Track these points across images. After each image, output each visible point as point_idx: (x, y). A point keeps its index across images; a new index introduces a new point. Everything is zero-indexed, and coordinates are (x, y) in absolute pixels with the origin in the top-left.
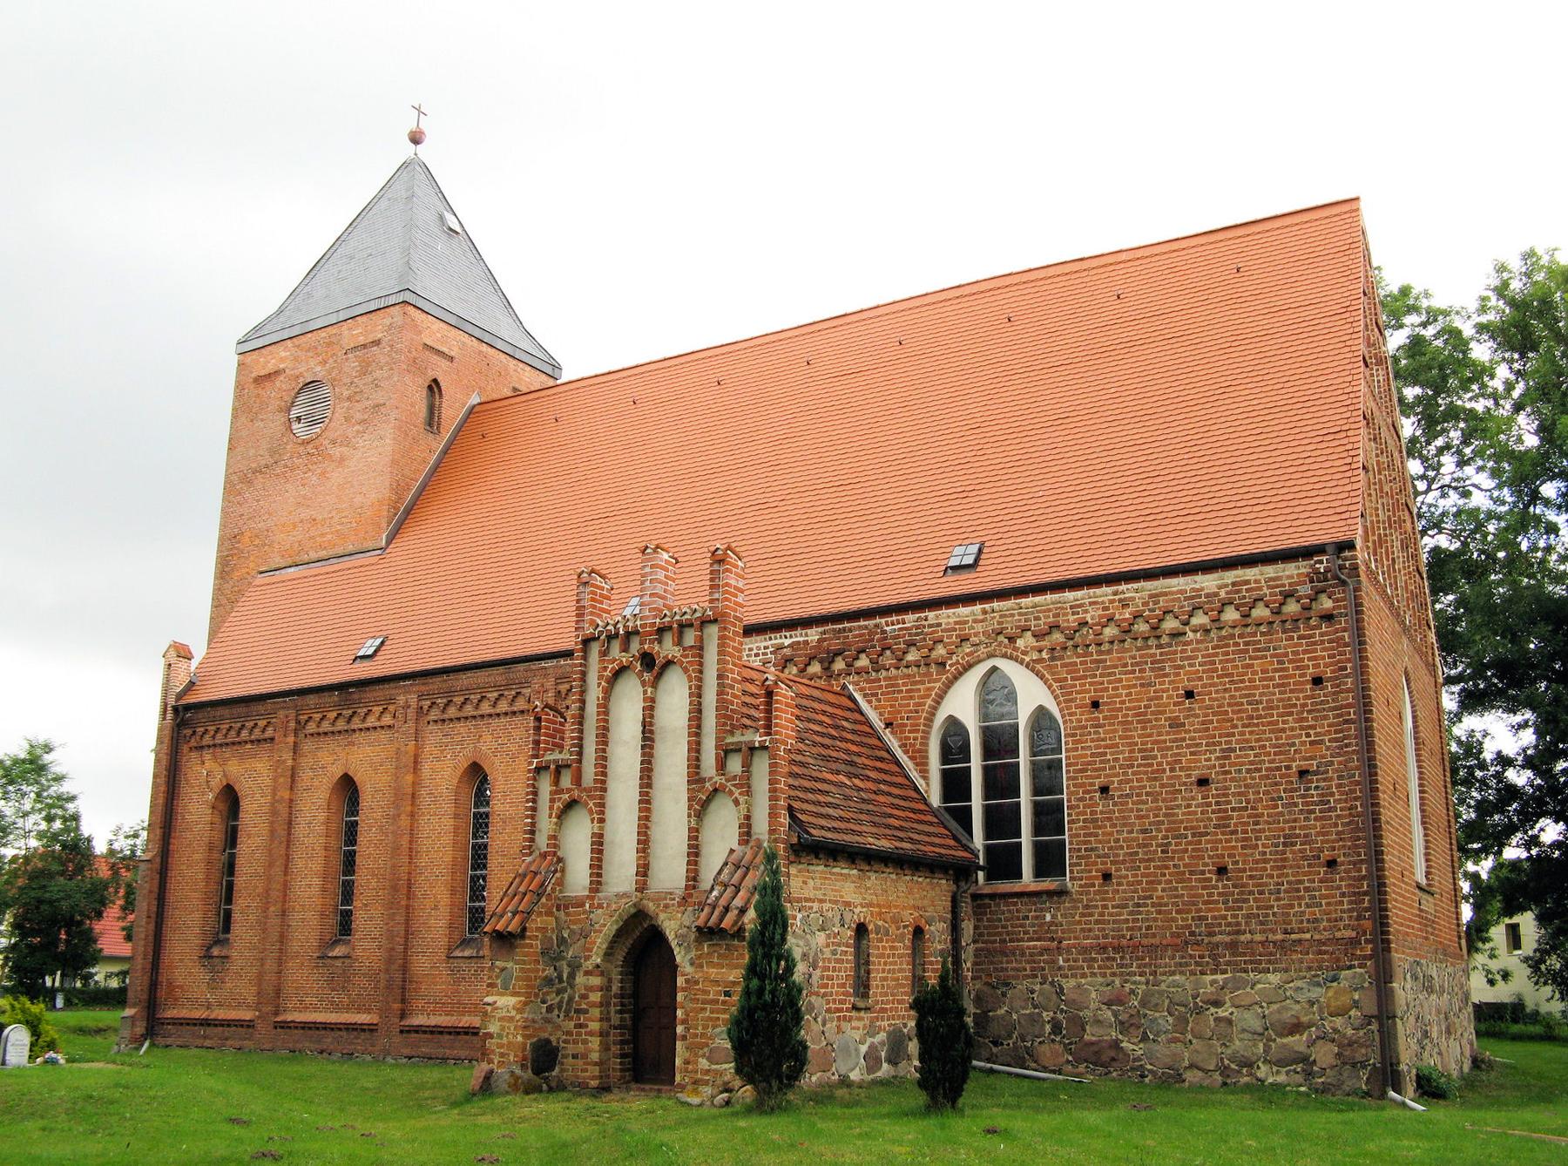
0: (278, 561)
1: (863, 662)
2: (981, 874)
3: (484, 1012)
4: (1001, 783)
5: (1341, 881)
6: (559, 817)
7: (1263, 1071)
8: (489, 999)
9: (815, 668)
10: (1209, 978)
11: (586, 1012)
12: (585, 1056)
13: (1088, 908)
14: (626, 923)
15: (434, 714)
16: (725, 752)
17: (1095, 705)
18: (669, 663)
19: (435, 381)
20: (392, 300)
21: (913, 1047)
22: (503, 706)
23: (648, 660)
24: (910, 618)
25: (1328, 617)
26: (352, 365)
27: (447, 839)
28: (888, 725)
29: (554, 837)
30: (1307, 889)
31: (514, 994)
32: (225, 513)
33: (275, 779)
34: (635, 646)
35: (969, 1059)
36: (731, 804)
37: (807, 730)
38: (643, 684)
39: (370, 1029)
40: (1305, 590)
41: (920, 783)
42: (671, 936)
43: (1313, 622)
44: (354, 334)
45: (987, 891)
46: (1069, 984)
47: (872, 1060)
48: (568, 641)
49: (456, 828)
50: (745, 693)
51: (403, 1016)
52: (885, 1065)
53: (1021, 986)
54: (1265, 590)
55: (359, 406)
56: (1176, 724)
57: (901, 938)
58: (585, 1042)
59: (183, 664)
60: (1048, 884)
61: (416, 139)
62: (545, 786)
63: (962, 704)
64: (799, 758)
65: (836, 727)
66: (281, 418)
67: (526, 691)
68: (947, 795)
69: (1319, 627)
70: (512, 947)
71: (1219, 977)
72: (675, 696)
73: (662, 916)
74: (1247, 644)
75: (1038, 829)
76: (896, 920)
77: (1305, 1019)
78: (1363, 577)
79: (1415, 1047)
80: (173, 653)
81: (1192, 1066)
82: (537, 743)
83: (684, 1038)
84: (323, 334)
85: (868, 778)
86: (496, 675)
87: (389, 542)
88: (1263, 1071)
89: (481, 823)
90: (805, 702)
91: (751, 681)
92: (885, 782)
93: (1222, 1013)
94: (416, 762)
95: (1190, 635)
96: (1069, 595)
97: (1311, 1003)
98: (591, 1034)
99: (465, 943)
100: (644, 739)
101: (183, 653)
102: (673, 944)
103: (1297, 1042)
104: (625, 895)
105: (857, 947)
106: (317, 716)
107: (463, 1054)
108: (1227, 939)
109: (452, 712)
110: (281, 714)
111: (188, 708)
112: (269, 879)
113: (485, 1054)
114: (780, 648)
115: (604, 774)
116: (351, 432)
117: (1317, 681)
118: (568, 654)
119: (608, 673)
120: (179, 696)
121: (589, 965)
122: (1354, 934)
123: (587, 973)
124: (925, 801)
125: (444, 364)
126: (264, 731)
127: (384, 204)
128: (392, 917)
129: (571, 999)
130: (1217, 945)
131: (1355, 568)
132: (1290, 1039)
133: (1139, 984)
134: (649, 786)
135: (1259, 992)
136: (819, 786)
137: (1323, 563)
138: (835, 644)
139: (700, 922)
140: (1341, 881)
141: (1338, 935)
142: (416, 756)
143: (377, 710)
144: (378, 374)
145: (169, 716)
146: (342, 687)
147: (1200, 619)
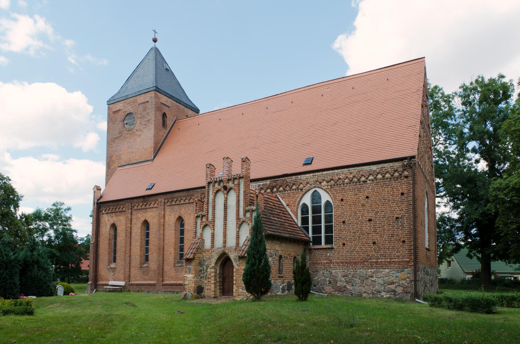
0: (123, 163)
1: (281, 189)
2: (311, 243)
3: (184, 279)
4: (317, 220)
5: (406, 246)
6: (203, 229)
7: (383, 294)
8: (185, 275)
9: (269, 191)
10: (370, 270)
11: (210, 278)
12: (210, 289)
13: (339, 252)
14: (220, 255)
15: (169, 204)
16: (246, 212)
17: (342, 200)
18: (231, 189)
20: (151, 89)
21: (293, 287)
22: (187, 201)
23: (225, 188)
24: (294, 177)
25: (406, 177)
26: (141, 108)
27: (173, 236)
28: (287, 205)
29: (202, 234)
32: (108, 150)
33: (126, 222)
34: (222, 184)
35: (310, 290)
36: (247, 225)
37: (267, 206)
38: (224, 194)
39: (154, 285)
40: (401, 169)
41: (296, 220)
42: (232, 258)
43: (402, 178)
44: (141, 99)
45: (313, 248)
46: (333, 271)
47: (283, 290)
48: (204, 183)
49: (175, 233)
50: (251, 196)
51: (163, 281)
52: (286, 292)
53: (321, 272)
54: (389, 169)
55: (144, 120)
56: (363, 205)
57: (291, 259)
58: (210, 286)
59: (99, 191)
60: (329, 246)
61: (155, 40)
62: (199, 221)
63: (307, 200)
64: (264, 213)
65: (274, 206)
66: (121, 123)
67: (193, 197)
68: (302, 224)
69: (404, 179)
70: (191, 262)
71: (373, 270)
72: (232, 197)
75: (326, 232)
76: (289, 255)
77: (395, 281)
78: (417, 166)
79: (423, 289)
80: (96, 189)
81: (365, 292)
82: (196, 210)
83: (235, 284)
84: (132, 99)
85: (283, 219)
86: (185, 193)
87: (154, 157)
88: (383, 294)
89: (182, 232)
90: (266, 199)
91: (252, 193)
92: (287, 220)
94: (164, 216)
95: (368, 182)
96: (336, 171)
97: (397, 277)
98: (212, 284)
99: (178, 263)
100: (225, 208)
101: (99, 189)
102: (233, 260)
103: (392, 287)
105: (280, 261)
106: (137, 205)
107: (178, 290)
108: (374, 260)
109: (173, 203)
110: (127, 204)
111: (101, 203)
112: (126, 248)
113: (185, 289)
114: (260, 185)
115: (214, 218)
117: (402, 194)
118: (204, 187)
119: (215, 191)
120: (98, 200)
121: (211, 266)
123: (211, 268)
124: (297, 225)
125: (167, 108)
126: (122, 208)
127: (146, 60)
128: (159, 256)
129: (206, 275)
130: (372, 262)
131: (415, 164)
133: (351, 272)
134: (226, 220)
135: (383, 274)
136: (270, 220)
137: (406, 162)
138: (274, 184)
139: (240, 255)
140: (406, 246)
141: (404, 260)
142: (164, 215)
143: (153, 203)
144: (148, 111)
145: (96, 205)
146: (143, 197)
147: (371, 177)
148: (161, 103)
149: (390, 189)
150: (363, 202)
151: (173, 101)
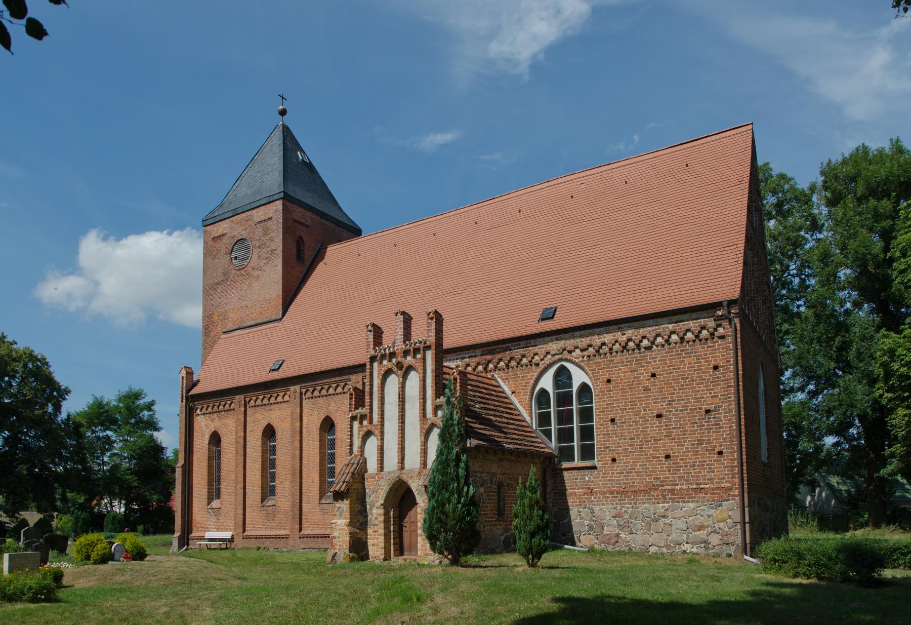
12: (377, 545)
15: (309, 394)
19: (301, 237)
23: (399, 365)
25: (722, 337)
26: (259, 230)
28: (513, 393)
30: (708, 465)
31: (345, 518)
41: (528, 419)
56: (646, 389)
61: (283, 113)
69: (717, 342)
71: (666, 505)
73: (410, 481)
74: (682, 351)
77: (705, 524)
93: (666, 521)
103: (702, 534)
104: (393, 472)
108: (669, 487)
116: (261, 264)
117: (716, 368)
122: (730, 485)
125: (304, 229)
132: (699, 533)
141: (722, 485)
148: (295, 221)
149: (693, 359)
150: (645, 383)
151: (314, 216)
